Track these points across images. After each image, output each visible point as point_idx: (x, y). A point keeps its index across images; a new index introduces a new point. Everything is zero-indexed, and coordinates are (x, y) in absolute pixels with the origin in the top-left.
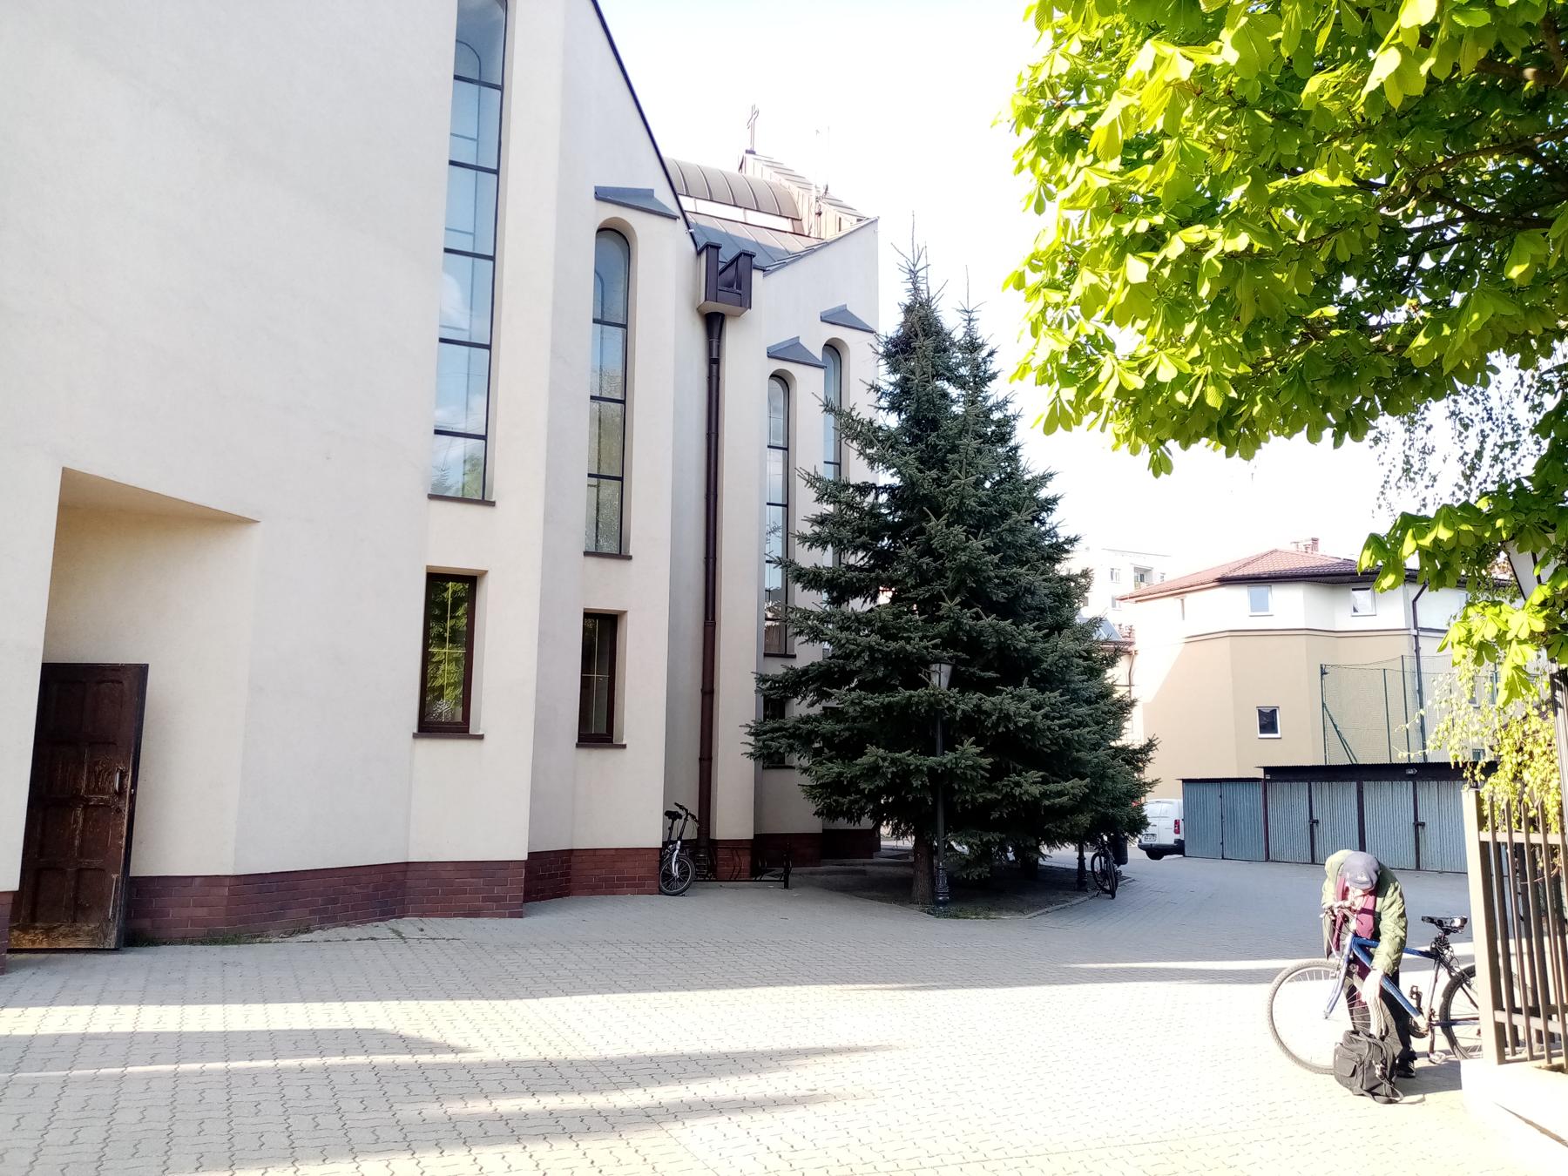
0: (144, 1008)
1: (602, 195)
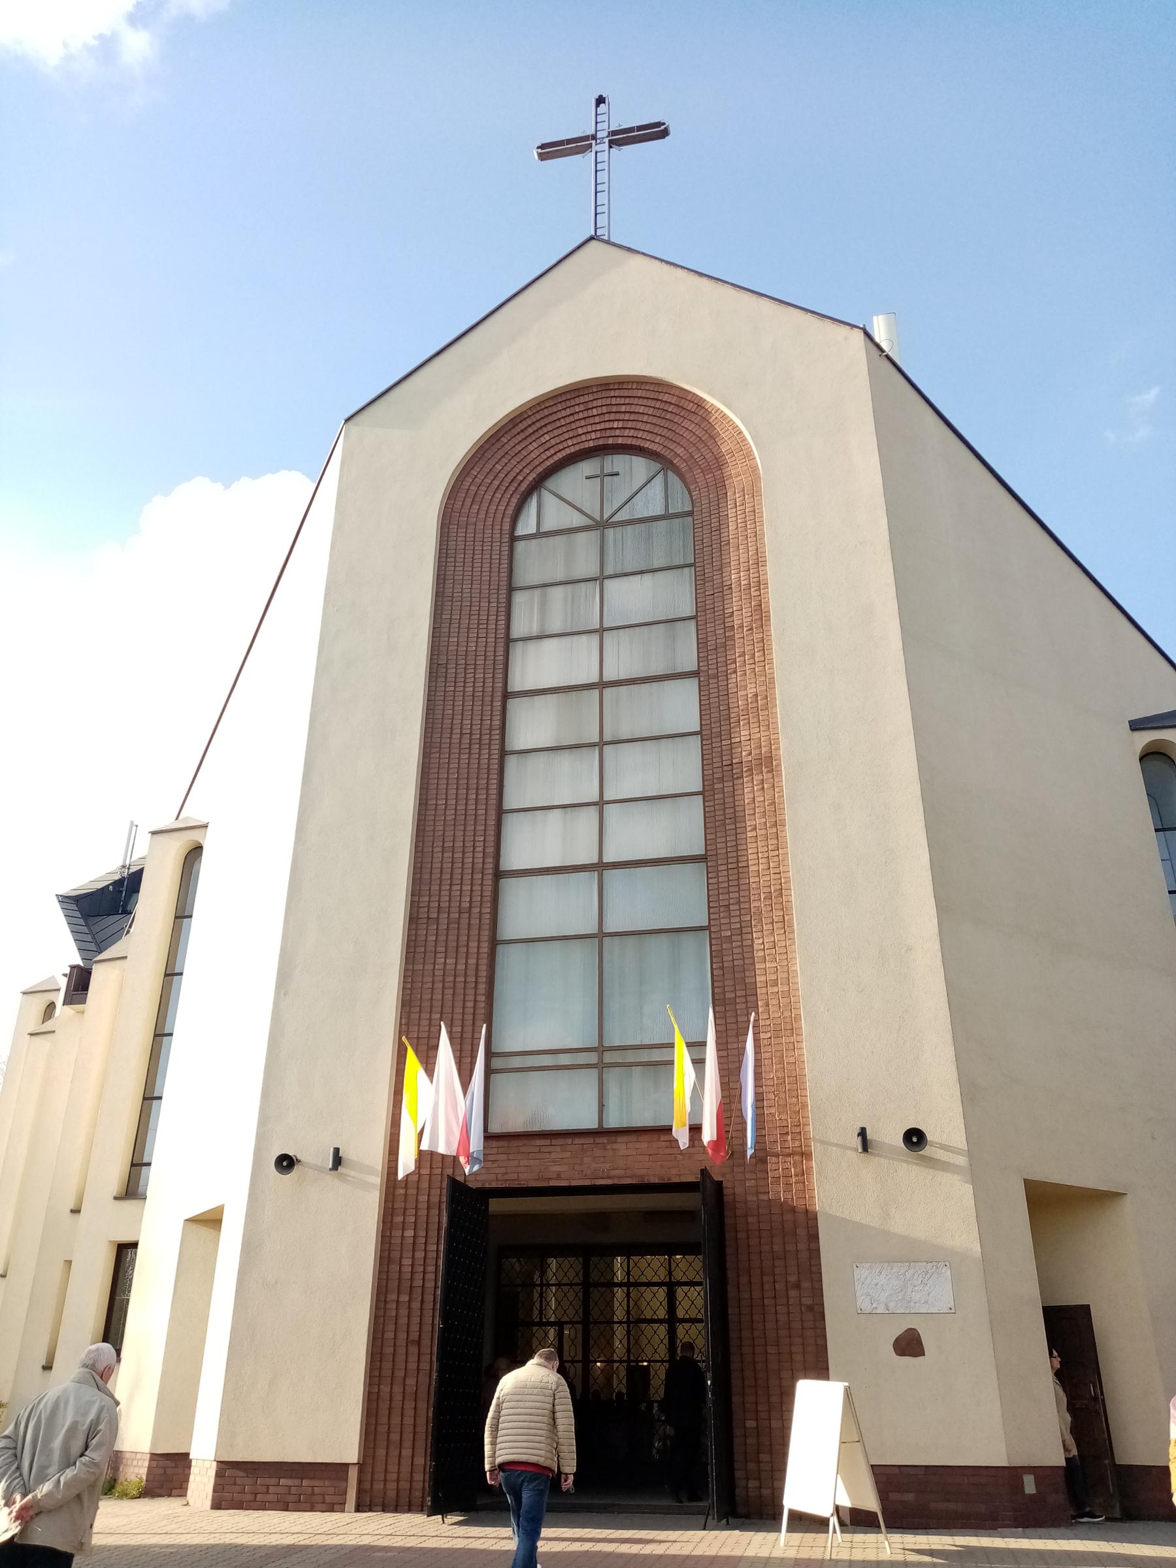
0: (821, 1558)
1: (1137, 726)
